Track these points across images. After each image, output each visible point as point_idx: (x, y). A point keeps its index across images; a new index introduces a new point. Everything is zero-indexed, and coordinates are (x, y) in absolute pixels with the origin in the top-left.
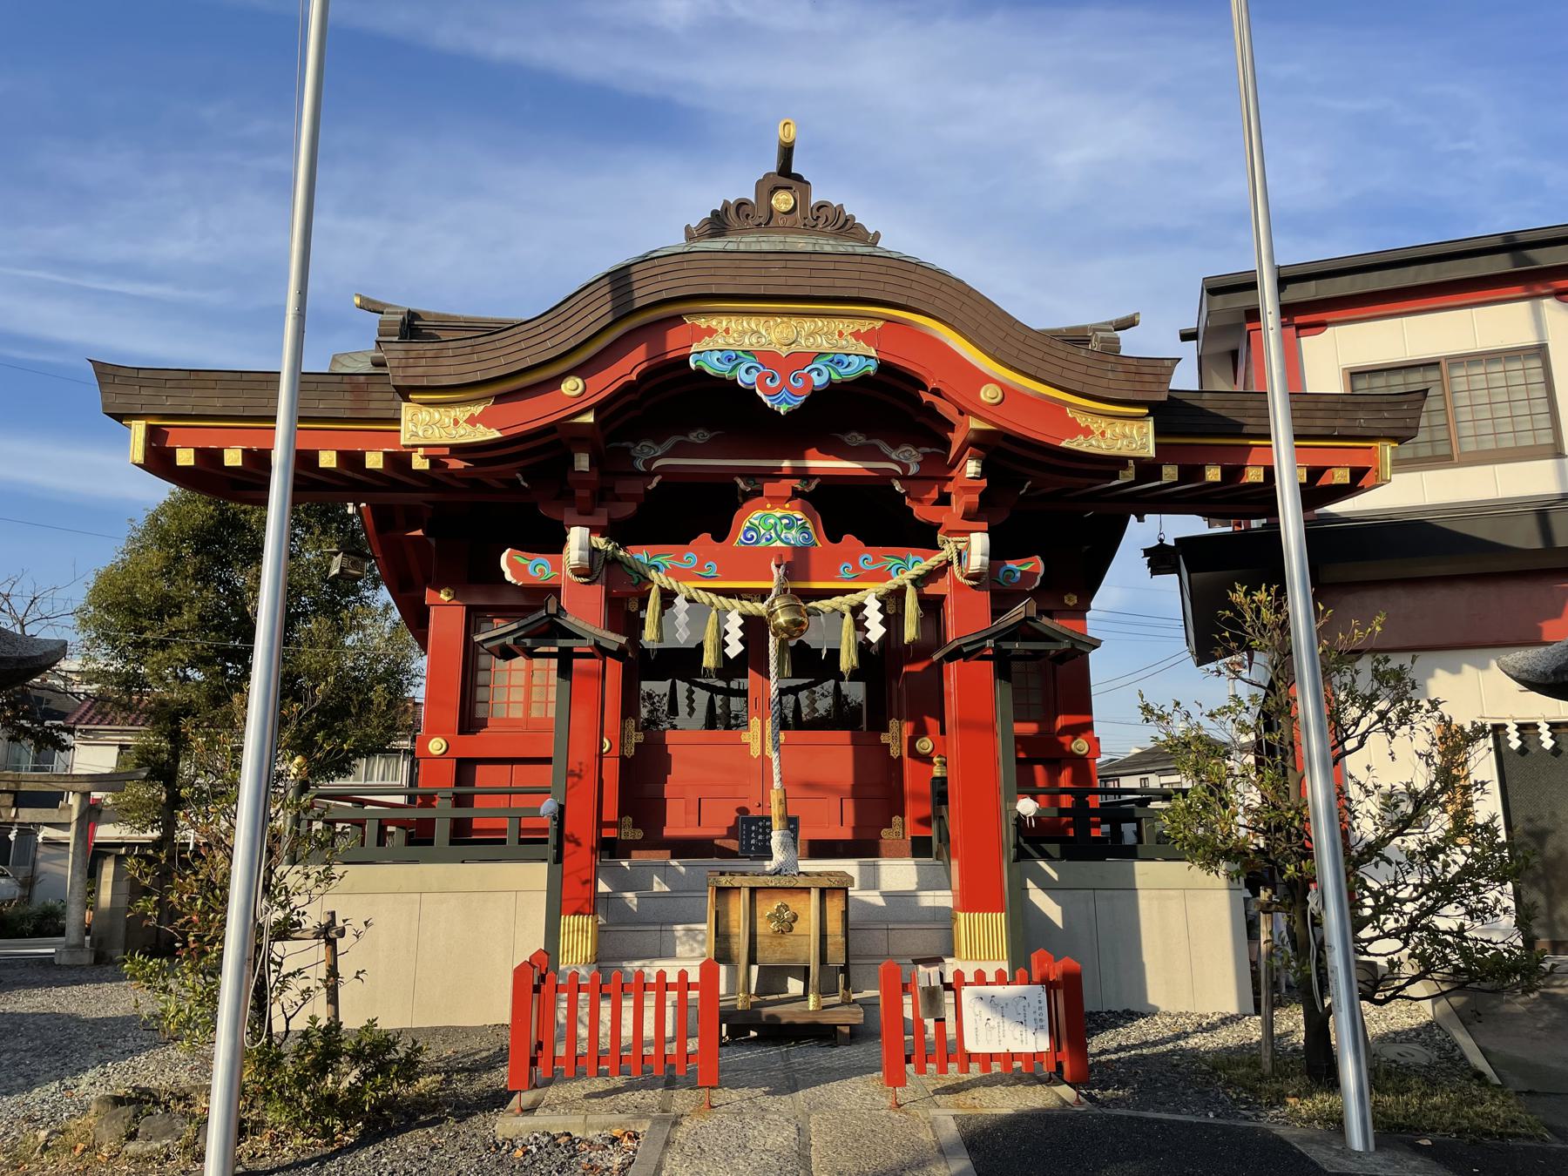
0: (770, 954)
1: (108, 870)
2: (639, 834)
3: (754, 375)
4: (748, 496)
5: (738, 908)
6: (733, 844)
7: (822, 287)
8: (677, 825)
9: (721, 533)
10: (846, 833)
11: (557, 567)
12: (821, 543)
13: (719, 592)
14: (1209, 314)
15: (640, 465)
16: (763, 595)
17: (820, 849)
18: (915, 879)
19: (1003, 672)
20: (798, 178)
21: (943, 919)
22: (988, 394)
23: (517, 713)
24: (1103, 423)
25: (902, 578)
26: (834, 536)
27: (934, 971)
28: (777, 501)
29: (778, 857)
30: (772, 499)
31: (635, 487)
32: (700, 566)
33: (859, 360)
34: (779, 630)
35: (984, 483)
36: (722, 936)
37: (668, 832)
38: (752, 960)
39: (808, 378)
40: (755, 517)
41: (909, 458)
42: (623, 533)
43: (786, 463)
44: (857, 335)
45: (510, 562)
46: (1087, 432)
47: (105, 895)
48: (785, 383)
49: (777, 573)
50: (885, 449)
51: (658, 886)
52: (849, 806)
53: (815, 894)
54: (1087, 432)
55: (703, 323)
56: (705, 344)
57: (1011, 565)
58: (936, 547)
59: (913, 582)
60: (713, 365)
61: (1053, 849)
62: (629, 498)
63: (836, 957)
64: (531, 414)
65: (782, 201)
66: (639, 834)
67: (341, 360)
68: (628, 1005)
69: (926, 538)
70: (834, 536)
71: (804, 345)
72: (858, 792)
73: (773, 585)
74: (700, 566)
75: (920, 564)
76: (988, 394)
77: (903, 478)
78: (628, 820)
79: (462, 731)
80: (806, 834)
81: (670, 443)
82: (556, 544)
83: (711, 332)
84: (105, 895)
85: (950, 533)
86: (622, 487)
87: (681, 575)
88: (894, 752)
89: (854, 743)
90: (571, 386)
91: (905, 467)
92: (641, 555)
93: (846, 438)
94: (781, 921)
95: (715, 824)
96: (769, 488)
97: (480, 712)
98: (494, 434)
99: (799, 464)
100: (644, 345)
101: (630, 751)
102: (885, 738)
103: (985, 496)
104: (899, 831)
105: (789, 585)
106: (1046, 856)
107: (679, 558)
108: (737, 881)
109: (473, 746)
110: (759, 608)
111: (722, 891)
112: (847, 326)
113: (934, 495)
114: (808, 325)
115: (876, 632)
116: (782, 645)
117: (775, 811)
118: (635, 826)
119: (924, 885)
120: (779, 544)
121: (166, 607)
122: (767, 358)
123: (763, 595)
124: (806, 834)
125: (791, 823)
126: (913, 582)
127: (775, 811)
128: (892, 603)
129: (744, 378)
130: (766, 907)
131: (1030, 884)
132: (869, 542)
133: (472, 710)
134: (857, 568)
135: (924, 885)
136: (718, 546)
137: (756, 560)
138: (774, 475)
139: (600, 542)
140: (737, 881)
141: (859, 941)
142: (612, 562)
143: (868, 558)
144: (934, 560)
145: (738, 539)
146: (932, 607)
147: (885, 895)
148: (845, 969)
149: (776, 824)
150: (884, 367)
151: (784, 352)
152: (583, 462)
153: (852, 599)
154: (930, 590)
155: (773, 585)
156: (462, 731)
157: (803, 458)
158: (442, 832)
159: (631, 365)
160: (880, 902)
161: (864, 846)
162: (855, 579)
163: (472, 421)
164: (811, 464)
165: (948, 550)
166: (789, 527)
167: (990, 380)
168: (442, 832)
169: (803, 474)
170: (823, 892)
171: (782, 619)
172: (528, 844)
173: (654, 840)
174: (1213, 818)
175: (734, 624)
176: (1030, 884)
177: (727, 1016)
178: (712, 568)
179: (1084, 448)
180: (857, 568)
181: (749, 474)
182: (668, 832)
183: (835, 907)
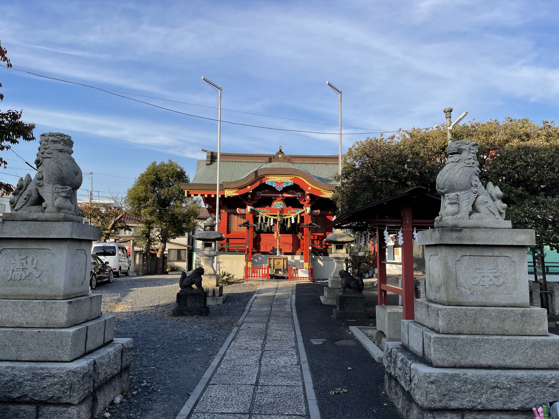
0: (276, 267)
1: (138, 256)
2: (256, 251)
3: (275, 185)
4: (274, 200)
5: (272, 261)
6: (272, 253)
7: (285, 173)
8: (262, 249)
9: (270, 205)
10: (291, 252)
11: (245, 211)
12: (285, 208)
13: (269, 215)
15: (258, 195)
16: (276, 216)
18: (300, 258)
19: (309, 230)
20: (282, 152)
21: (303, 263)
22: (309, 188)
23: (236, 231)
24: (326, 193)
26: (287, 206)
27: (295, 267)
28: (279, 201)
29: (278, 254)
30: (278, 200)
31: (257, 198)
32: (267, 211)
33: (291, 183)
34: (278, 221)
35: (310, 199)
36: (270, 265)
37: (261, 251)
38: (274, 268)
39: (283, 186)
40: (275, 203)
41: (299, 194)
43: (280, 195)
44: (290, 179)
45: (238, 210)
46: (324, 194)
47: (137, 262)
48: (280, 187)
49: (278, 212)
50: (296, 193)
51: (260, 259)
52: (291, 247)
53: (283, 259)
54: (324, 194)
55: (268, 177)
56: (268, 180)
57: (315, 211)
58: (303, 208)
59: (299, 214)
60: (269, 184)
61: (322, 254)
62: (256, 200)
63: (285, 268)
64: (243, 192)
65: (280, 156)
66: (256, 251)
67: (200, 162)
68: (261, 270)
69: (301, 207)
70: (287, 206)
71: (283, 181)
72: (293, 245)
73: (278, 214)
74: (267, 211)
75: (300, 211)
76: (309, 188)
77: (298, 197)
78: (254, 248)
79: (227, 234)
80: (283, 251)
81: (262, 192)
82: (245, 207)
83: (269, 179)
84: (137, 262)
85: (305, 206)
86: (255, 199)
87: (264, 212)
88: (299, 238)
89: (292, 236)
90: (249, 187)
91: (299, 196)
92: (258, 209)
93: (290, 191)
94: (278, 263)
95: (269, 249)
96: (277, 199)
97: (229, 231)
98: (238, 194)
99: (282, 195)
101: (254, 237)
102: (298, 235)
103: (310, 201)
104: (299, 251)
105: (280, 214)
106: (321, 255)
107: (263, 210)
108: (272, 257)
109: (229, 236)
110: (276, 218)
111: (270, 259)
112: (289, 178)
113: (303, 200)
114: (283, 178)
115: (293, 222)
116: (279, 224)
117: (278, 248)
118: (255, 249)
119: (301, 259)
120: (279, 208)
121: (146, 199)
122: (277, 183)
123: (276, 216)
124: (283, 251)
125: (280, 250)
126: (299, 214)
127: (278, 248)
129: (274, 186)
130: (276, 261)
131: (318, 259)
132: (293, 207)
133: (228, 230)
134: (291, 212)
135: (301, 259)
136: (270, 208)
137: (275, 210)
138: (278, 197)
139: (252, 208)
140: (272, 257)
141: (289, 267)
142: (254, 211)
143: (292, 210)
144: (302, 211)
145: (273, 207)
147: (294, 261)
148: (287, 270)
149: (278, 250)
150: (294, 184)
151: (280, 182)
152: (250, 196)
153: (290, 216)
154: (302, 215)
155: (278, 214)
156: (227, 234)
157: (283, 194)
158: (226, 250)
159: (257, 184)
160: (294, 262)
161: (293, 254)
162: (290, 213)
163: (235, 192)
164: (284, 195)
165: (304, 209)
166: (280, 205)
167: (310, 186)
168: (226, 250)
169: (283, 197)
170: (284, 259)
171: (279, 220)
172: (241, 252)
173: (258, 252)
175: (272, 220)
176: (318, 259)
177: (270, 275)
178: (268, 211)
179: (323, 197)
180: (291, 212)
181: (275, 197)
182: (261, 251)
183: (285, 261)
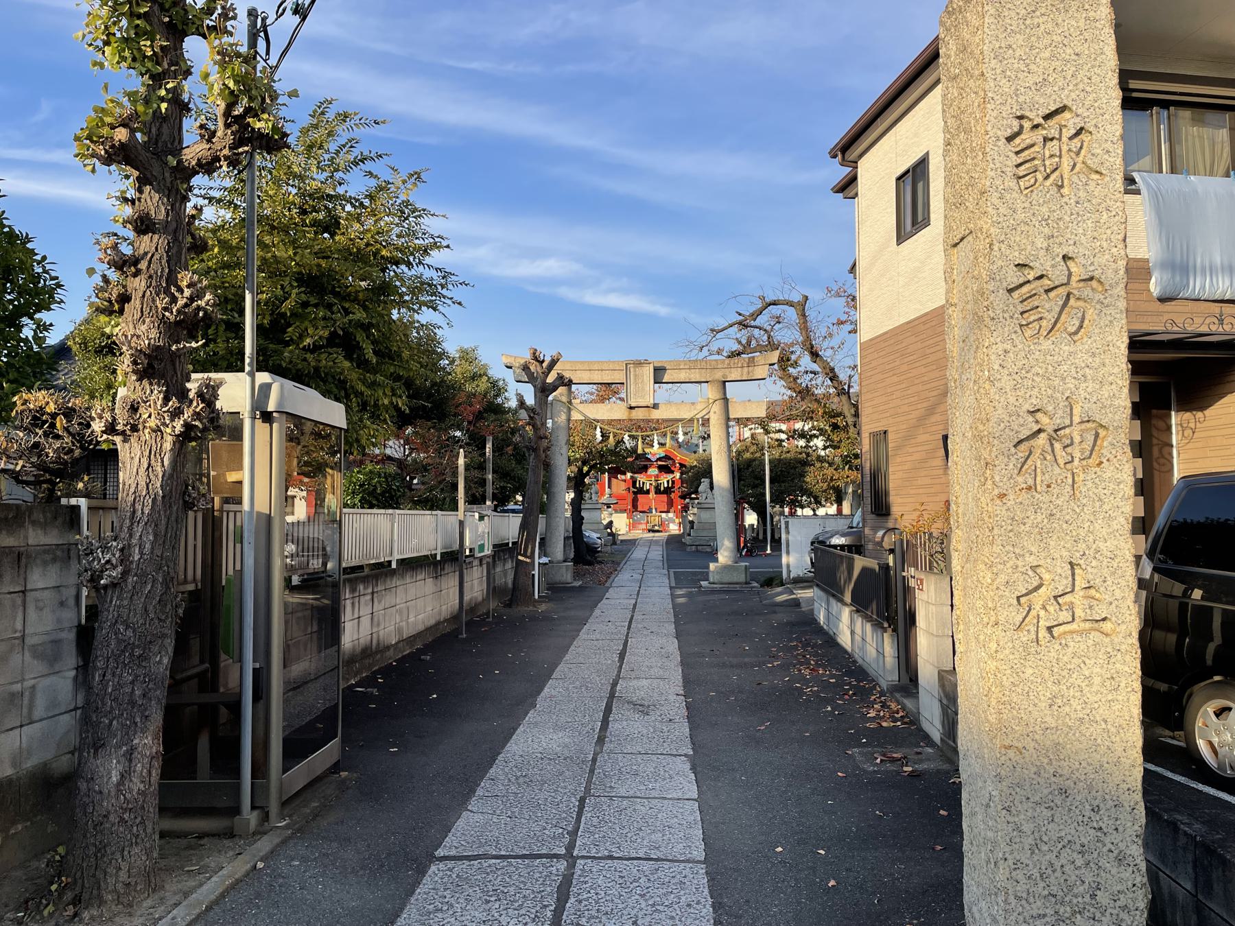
41: (671, 462)
69: (672, 472)
75: (671, 476)
104: (672, 510)
128: (668, 482)
145: (649, 473)
146: (673, 482)
161: (668, 512)
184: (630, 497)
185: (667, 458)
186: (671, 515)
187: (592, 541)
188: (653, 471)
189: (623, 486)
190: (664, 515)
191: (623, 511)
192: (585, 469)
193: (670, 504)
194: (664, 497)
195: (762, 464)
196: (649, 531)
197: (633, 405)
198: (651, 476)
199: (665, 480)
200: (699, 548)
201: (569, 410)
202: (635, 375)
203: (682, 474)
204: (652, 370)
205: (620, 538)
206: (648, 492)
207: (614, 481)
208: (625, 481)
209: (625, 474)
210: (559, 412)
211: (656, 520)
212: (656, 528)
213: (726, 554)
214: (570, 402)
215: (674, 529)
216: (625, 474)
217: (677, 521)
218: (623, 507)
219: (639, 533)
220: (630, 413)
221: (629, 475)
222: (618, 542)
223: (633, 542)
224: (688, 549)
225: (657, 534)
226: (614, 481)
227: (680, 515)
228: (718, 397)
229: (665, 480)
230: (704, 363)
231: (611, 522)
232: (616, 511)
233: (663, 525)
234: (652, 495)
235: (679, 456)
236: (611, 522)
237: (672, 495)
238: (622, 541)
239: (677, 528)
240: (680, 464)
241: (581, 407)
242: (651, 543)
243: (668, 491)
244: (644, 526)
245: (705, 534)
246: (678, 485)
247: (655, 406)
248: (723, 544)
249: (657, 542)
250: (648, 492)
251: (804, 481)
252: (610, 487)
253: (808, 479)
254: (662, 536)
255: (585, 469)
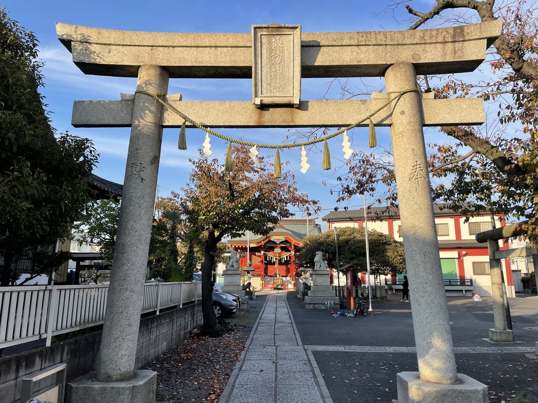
14: (259, 312)
17: (282, 276)
25: (288, 255)
33: (284, 240)
41: (289, 244)
42: (265, 251)
64: (260, 244)
69: (290, 251)
75: (289, 253)
76: (293, 242)
92: (267, 253)
95: (273, 274)
100: (316, 64)
104: (289, 275)
115: (285, 259)
122: (277, 239)
125: (279, 274)
128: (287, 257)
130: (277, 280)
145: (275, 252)
146: (290, 257)
161: (286, 276)
173: (267, 275)
174: (222, 355)
184: (263, 266)
185: (286, 242)
186: (288, 278)
187: (229, 303)
188: (277, 250)
189: (259, 259)
190: (284, 278)
191: (258, 275)
192: (217, 234)
193: (288, 271)
194: (284, 267)
195: (364, 241)
196: (275, 289)
197: (267, 101)
198: (276, 253)
199: (285, 256)
200: (316, 306)
201: (161, 109)
202: (271, 51)
203: (296, 252)
204: (298, 48)
205: (256, 294)
206: (274, 264)
207: (253, 257)
208: (260, 256)
209: (260, 252)
210: (143, 110)
211: (279, 282)
212: (279, 287)
213: (437, 363)
214: (163, 97)
215: (291, 287)
216: (260, 252)
217: (293, 282)
218: (259, 273)
219: (269, 291)
220: (260, 117)
221: (262, 252)
222: (254, 297)
223: (263, 298)
224: (307, 307)
225: (280, 291)
226: (253, 257)
227: (294, 278)
228: (406, 88)
229: (285, 256)
230: (381, 37)
231: (249, 284)
232: (254, 276)
233: (283, 286)
234: (276, 266)
235: (294, 241)
236: (249, 284)
237: (289, 266)
238: (257, 296)
239: (293, 287)
240: (294, 246)
241: (180, 106)
242: (277, 298)
243: (287, 263)
244: (271, 286)
245: (320, 294)
246: (293, 259)
247: (302, 106)
248: (430, 345)
249: (281, 297)
250: (274, 264)
251: (386, 256)
252: (250, 260)
253: (389, 254)
254: (283, 293)
255: (217, 234)
